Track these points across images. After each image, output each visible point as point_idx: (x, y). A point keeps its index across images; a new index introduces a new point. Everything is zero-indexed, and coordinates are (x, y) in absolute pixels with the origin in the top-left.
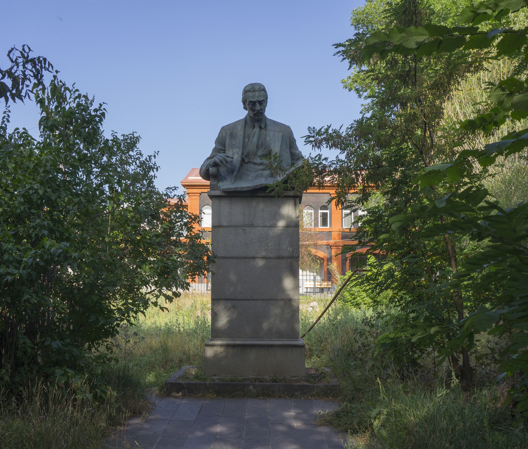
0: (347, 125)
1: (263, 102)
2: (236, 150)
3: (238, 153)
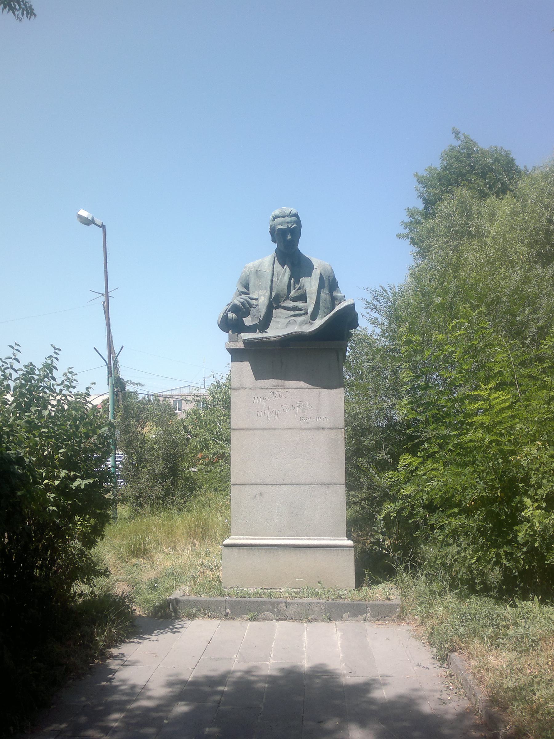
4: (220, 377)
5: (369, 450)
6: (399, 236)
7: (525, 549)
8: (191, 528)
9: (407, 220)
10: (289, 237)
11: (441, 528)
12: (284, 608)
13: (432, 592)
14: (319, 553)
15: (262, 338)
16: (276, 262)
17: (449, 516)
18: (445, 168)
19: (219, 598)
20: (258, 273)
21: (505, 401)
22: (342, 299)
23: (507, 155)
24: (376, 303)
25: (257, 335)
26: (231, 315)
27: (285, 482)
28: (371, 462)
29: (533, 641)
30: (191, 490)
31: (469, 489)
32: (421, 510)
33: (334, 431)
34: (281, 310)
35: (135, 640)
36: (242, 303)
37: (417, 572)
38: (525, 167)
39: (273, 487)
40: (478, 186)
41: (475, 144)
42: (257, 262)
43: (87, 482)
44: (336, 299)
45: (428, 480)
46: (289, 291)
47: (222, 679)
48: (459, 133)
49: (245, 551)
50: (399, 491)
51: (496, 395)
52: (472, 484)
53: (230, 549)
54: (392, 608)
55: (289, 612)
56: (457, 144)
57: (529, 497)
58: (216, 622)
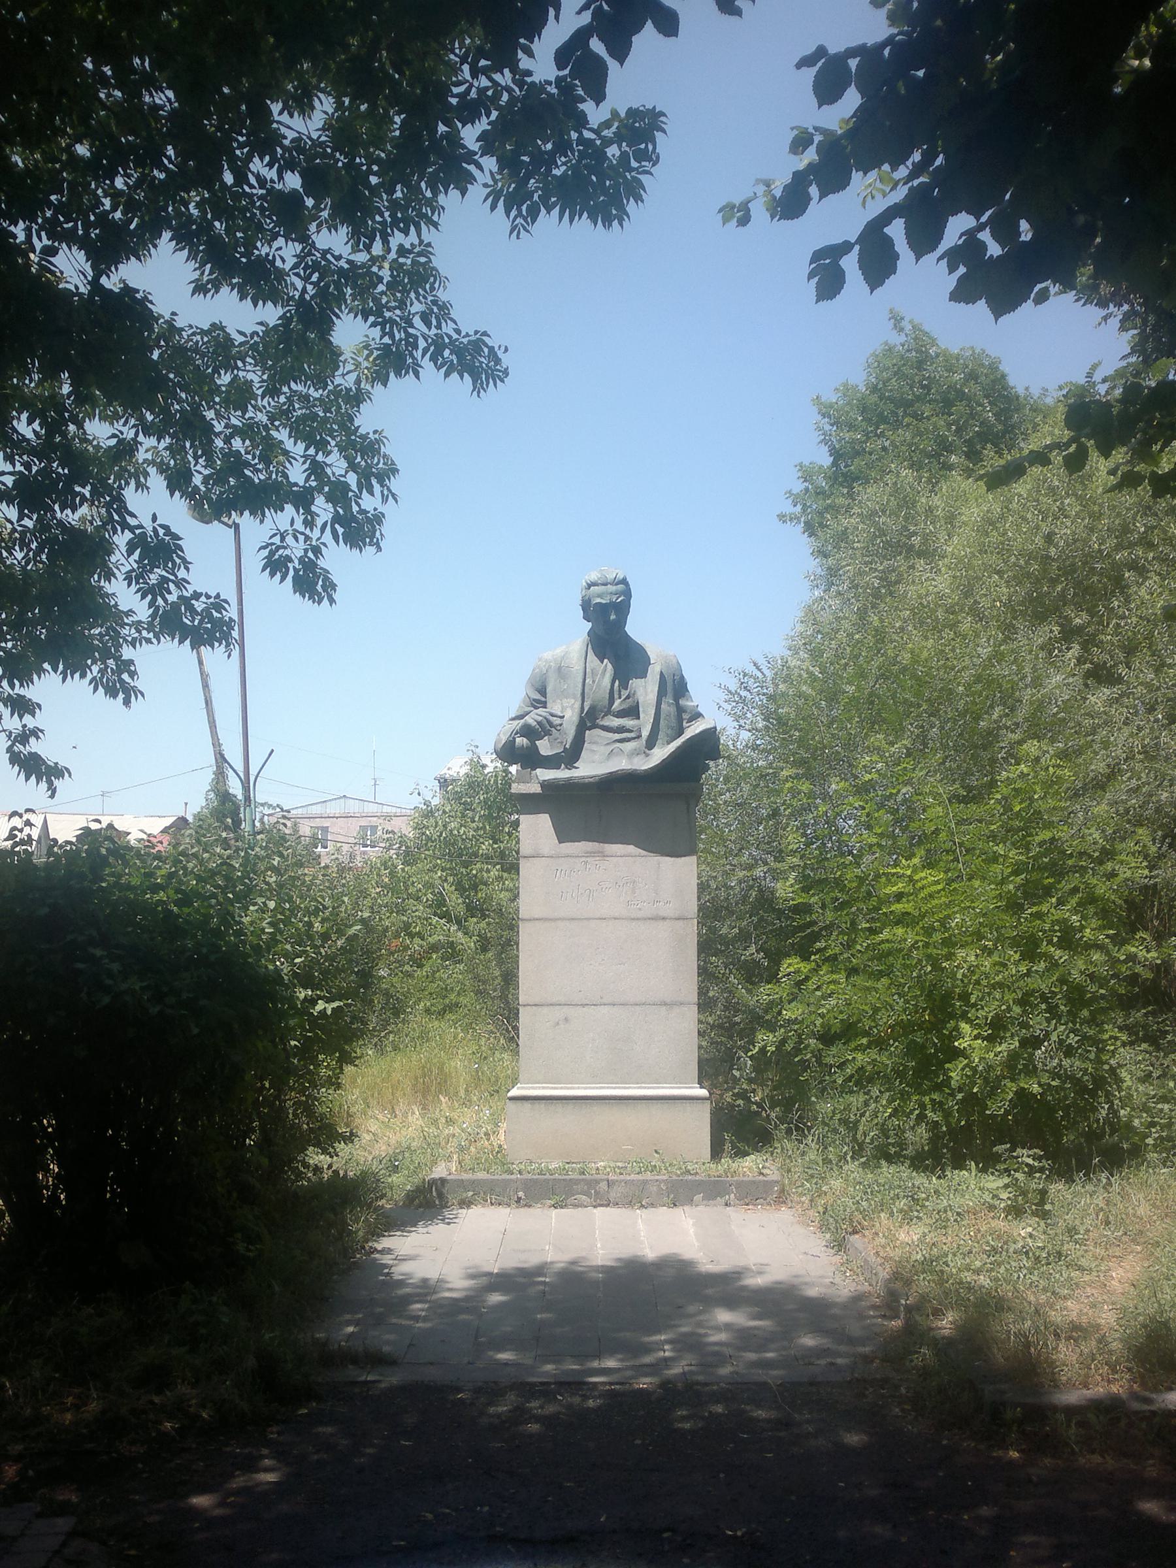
0: (1052, 386)
1: (622, 608)
2: (566, 702)
3: (572, 707)
4: (431, 794)
5: (727, 945)
6: (782, 517)
7: (960, 1096)
8: (416, 1078)
9: (798, 487)
10: (613, 617)
11: (842, 1066)
12: (606, 1188)
13: (827, 1161)
14: (655, 1109)
15: (570, 779)
16: (590, 652)
17: (856, 1049)
18: (874, 389)
19: (506, 1176)
20: (561, 671)
21: (937, 882)
22: (697, 716)
23: (994, 367)
24: (743, 693)
25: (562, 774)
26: (521, 741)
27: (605, 1001)
28: (731, 963)
29: (958, 1214)
30: (396, 1014)
31: (883, 1010)
32: (812, 1041)
33: (680, 923)
34: (597, 732)
35: (398, 1233)
36: (539, 723)
37: (805, 1137)
38: (1027, 389)
39: (586, 1009)
40: (935, 428)
41: (934, 342)
42: (559, 651)
43: (335, 1004)
44: (685, 711)
45: (824, 997)
46: (612, 701)
47: (540, 1270)
48: (902, 319)
49: (542, 1105)
50: (780, 1013)
51: (923, 875)
52: (887, 1003)
53: (519, 1103)
54: (769, 1185)
55: (613, 1195)
56: (897, 339)
57: (970, 1021)
58: (504, 1211)
